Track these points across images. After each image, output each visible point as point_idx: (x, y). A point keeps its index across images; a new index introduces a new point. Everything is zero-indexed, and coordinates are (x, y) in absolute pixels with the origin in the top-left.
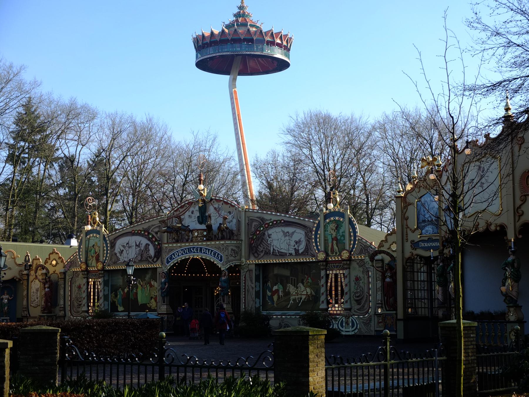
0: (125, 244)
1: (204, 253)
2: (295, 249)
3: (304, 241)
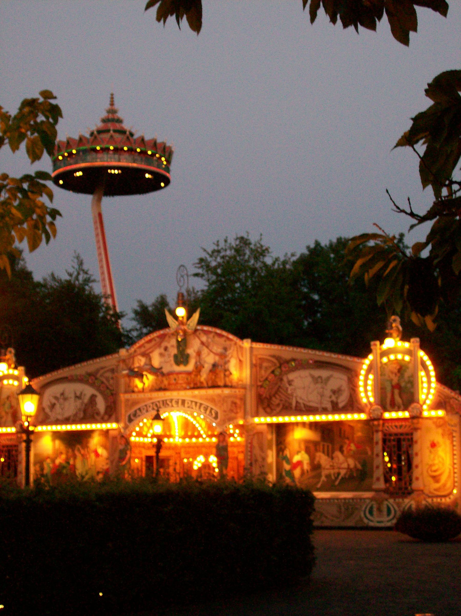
0: (58, 395)
1: (188, 407)
2: (332, 402)
3: (347, 389)
